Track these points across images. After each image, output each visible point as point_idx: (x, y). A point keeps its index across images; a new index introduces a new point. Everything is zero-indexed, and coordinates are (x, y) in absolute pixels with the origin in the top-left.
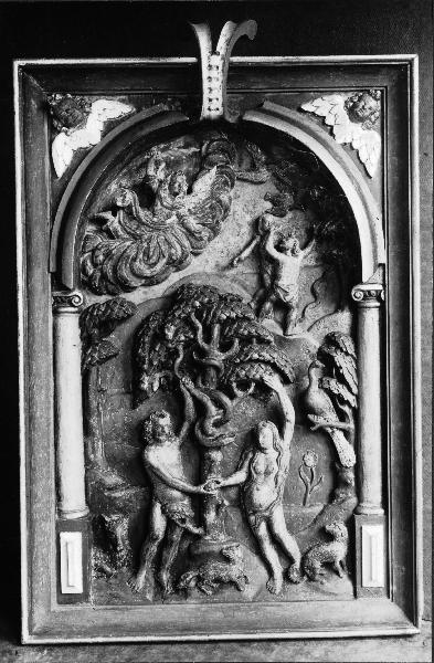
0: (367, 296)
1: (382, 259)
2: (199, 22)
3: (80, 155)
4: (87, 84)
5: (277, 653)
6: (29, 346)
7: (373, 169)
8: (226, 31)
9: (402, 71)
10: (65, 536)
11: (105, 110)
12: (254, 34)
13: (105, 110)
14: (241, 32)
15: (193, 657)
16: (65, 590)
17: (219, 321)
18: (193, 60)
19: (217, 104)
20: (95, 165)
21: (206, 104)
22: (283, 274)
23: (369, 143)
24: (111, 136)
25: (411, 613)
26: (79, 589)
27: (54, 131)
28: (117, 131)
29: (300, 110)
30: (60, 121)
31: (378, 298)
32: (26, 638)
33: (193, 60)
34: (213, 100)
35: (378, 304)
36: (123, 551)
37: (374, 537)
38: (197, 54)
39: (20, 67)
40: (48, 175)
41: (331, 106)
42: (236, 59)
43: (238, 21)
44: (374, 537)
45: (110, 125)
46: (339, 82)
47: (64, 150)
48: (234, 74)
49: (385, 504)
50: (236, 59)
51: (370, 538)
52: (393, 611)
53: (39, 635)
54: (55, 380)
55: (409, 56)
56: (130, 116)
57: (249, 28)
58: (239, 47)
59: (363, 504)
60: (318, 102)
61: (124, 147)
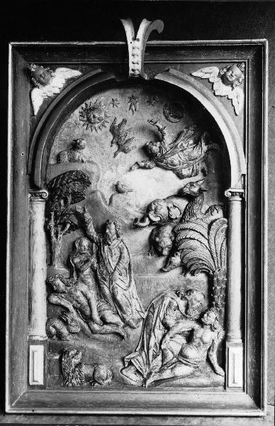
0: (233, 194)
1: (106, 247)
2: (125, 18)
3: (48, 102)
4: (52, 60)
5: (169, 422)
6: (14, 225)
7: (239, 108)
8: (144, 25)
9: (259, 49)
10: (32, 348)
11: (60, 78)
12: (162, 29)
13: (60, 78)
14: (153, 27)
15: (116, 422)
16: (31, 384)
17: (138, 40)
18: (124, 43)
19: (139, 67)
20: (58, 108)
21: (131, 66)
22: (176, 191)
23: (237, 95)
24: (69, 88)
25: (258, 403)
26: (41, 382)
27: (34, 86)
28: (74, 84)
29: (191, 75)
30: (33, 81)
31: (241, 196)
32: (8, 409)
33: (124, 43)
34: (136, 62)
35: (240, 199)
36: (108, 202)
37: (236, 353)
38: (125, 39)
39: (13, 46)
40: (29, 112)
41: (212, 72)
42: (150, 42)
43: (151, 19)
44: (236, 353)
45: (69, 81)
46: (214, 57)
47: (39, 97)
48: (149, 50)
49: (243, 338)
50: (150, 42)
51: (234, 355)
52: (247, 399)
53: (19, 404)
54: (30, 252)
55: (262, 40)
56: (79, 77)
57: (159, 25)
58: (153, 35)
59: (229, 334)
60: (207, 69)
61: (76, 94)
